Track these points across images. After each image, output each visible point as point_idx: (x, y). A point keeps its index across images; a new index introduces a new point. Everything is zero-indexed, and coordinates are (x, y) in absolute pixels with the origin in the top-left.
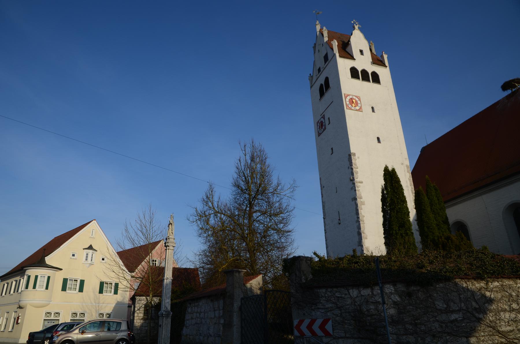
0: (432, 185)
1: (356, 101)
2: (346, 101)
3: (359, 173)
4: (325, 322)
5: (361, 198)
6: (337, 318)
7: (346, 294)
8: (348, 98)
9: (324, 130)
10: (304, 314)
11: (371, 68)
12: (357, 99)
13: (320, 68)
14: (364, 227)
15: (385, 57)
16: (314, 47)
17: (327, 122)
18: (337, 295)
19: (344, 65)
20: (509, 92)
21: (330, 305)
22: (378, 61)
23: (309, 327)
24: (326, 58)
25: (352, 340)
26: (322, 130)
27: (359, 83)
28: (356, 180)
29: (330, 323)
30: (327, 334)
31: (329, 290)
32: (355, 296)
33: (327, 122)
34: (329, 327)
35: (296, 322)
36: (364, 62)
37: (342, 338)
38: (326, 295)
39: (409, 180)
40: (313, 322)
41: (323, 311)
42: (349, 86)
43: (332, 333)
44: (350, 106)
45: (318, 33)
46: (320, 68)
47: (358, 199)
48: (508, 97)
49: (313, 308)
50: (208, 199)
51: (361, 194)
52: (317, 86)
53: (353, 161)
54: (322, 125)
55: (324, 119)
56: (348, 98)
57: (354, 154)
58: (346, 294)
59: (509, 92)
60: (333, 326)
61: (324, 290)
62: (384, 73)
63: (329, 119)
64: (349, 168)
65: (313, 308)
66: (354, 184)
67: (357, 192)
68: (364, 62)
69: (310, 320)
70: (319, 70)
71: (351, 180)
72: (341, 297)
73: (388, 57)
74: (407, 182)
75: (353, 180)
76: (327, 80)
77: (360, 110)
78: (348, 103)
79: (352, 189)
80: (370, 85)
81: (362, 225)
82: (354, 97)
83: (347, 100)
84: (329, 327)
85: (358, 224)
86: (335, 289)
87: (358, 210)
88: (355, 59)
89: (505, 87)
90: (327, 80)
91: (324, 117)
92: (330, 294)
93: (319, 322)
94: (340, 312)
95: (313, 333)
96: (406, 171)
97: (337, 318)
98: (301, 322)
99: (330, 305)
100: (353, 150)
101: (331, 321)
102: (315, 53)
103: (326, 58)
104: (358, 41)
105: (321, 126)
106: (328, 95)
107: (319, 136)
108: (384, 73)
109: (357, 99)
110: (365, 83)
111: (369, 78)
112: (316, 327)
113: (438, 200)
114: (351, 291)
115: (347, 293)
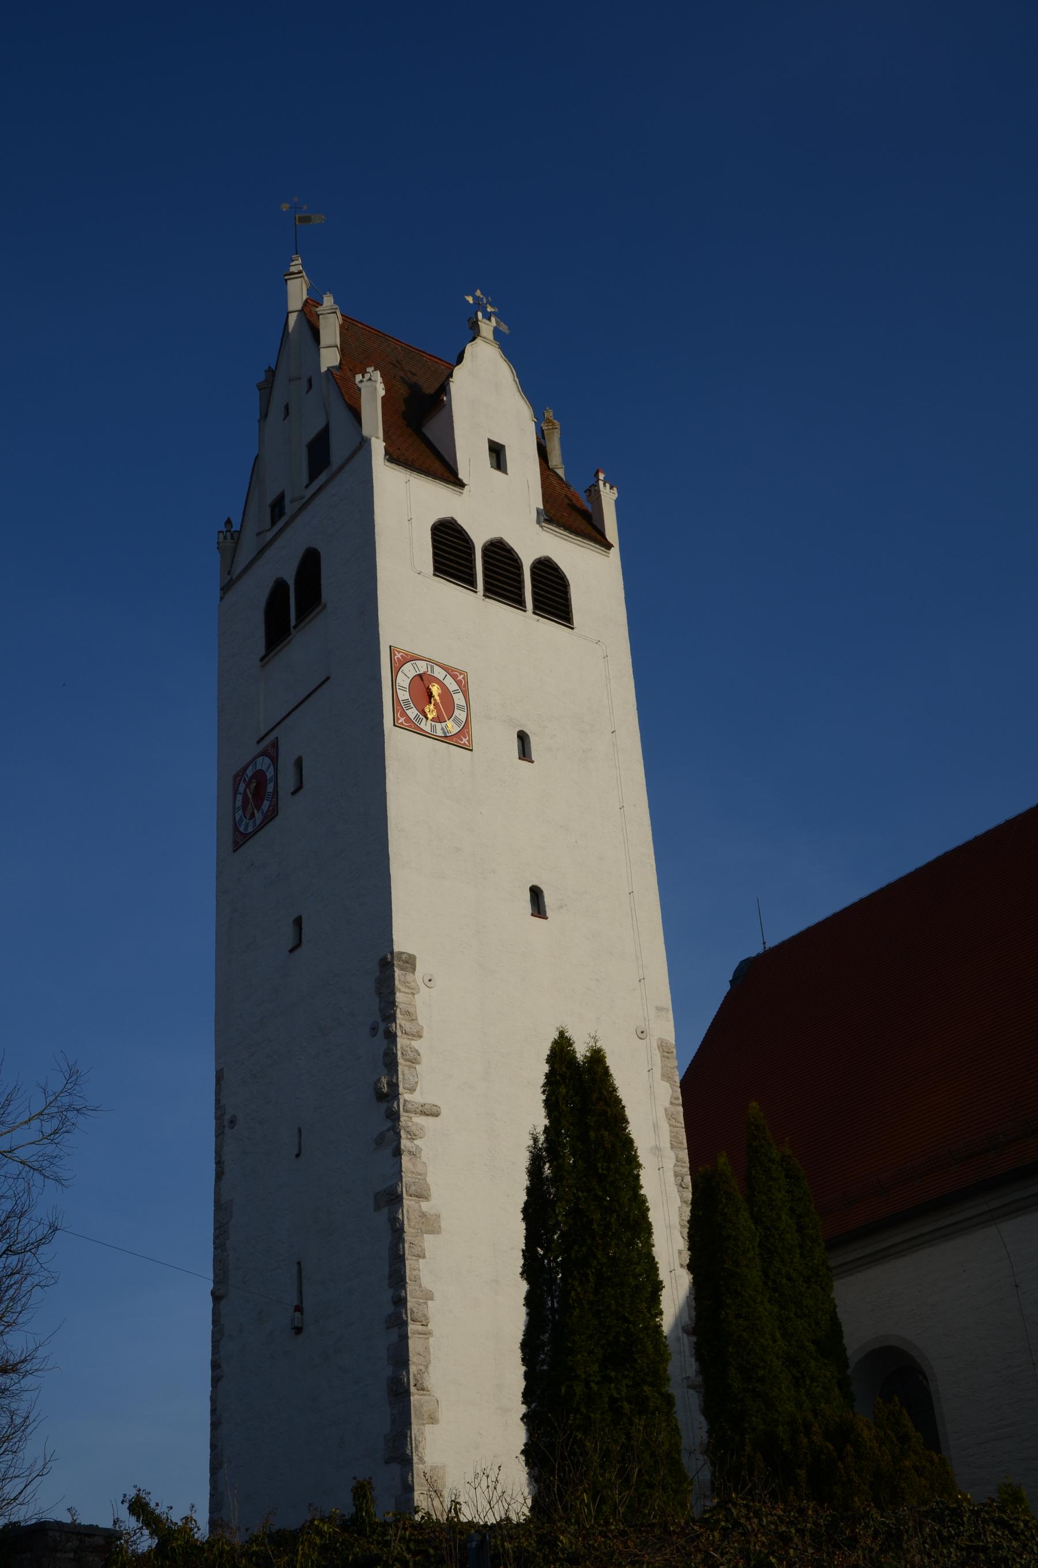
1: (446, 693)
2: (395, 686)
3: (424, 1059)
5: (423, 1195)
8: (409, 671)
11: (534, 544)
12: (451, 685)
15: (608, 497)
17: (287, 781)
24: (319, 453)
26: (259, 816)
27: (468, 606)
28: (405, 1096)
36: (503, 507)
39: (670, 1117)
42: (417, 613)
44: (412, 713)
45: (293, 319)
47: (408, 1202)
51: (423, 1175)
54: (259, 794)
56: (409, 671)
57: (410, 962)
62: (595, 576)
64: (374, 1030)
66: (394, 1117)
67: (405, 1159)
68: (503, 507)
70: (277, 507)
71: (381, 1097)
74: (656, 1127)
75: (393, 1093)
76: (310, 564)
77: (461, 740)
78: (404, 695)
79: (380, 1141)
80: (521, 625)
82: (439, 673)
88: (461, 485)
90: (310, 564)
91: (272, 753)
96: (658, 1071)
102: (264, 415)
103: (319, 453)
105: (253, 797)
106: (305, 644)
107: (237, 846)
110: (500, 611)
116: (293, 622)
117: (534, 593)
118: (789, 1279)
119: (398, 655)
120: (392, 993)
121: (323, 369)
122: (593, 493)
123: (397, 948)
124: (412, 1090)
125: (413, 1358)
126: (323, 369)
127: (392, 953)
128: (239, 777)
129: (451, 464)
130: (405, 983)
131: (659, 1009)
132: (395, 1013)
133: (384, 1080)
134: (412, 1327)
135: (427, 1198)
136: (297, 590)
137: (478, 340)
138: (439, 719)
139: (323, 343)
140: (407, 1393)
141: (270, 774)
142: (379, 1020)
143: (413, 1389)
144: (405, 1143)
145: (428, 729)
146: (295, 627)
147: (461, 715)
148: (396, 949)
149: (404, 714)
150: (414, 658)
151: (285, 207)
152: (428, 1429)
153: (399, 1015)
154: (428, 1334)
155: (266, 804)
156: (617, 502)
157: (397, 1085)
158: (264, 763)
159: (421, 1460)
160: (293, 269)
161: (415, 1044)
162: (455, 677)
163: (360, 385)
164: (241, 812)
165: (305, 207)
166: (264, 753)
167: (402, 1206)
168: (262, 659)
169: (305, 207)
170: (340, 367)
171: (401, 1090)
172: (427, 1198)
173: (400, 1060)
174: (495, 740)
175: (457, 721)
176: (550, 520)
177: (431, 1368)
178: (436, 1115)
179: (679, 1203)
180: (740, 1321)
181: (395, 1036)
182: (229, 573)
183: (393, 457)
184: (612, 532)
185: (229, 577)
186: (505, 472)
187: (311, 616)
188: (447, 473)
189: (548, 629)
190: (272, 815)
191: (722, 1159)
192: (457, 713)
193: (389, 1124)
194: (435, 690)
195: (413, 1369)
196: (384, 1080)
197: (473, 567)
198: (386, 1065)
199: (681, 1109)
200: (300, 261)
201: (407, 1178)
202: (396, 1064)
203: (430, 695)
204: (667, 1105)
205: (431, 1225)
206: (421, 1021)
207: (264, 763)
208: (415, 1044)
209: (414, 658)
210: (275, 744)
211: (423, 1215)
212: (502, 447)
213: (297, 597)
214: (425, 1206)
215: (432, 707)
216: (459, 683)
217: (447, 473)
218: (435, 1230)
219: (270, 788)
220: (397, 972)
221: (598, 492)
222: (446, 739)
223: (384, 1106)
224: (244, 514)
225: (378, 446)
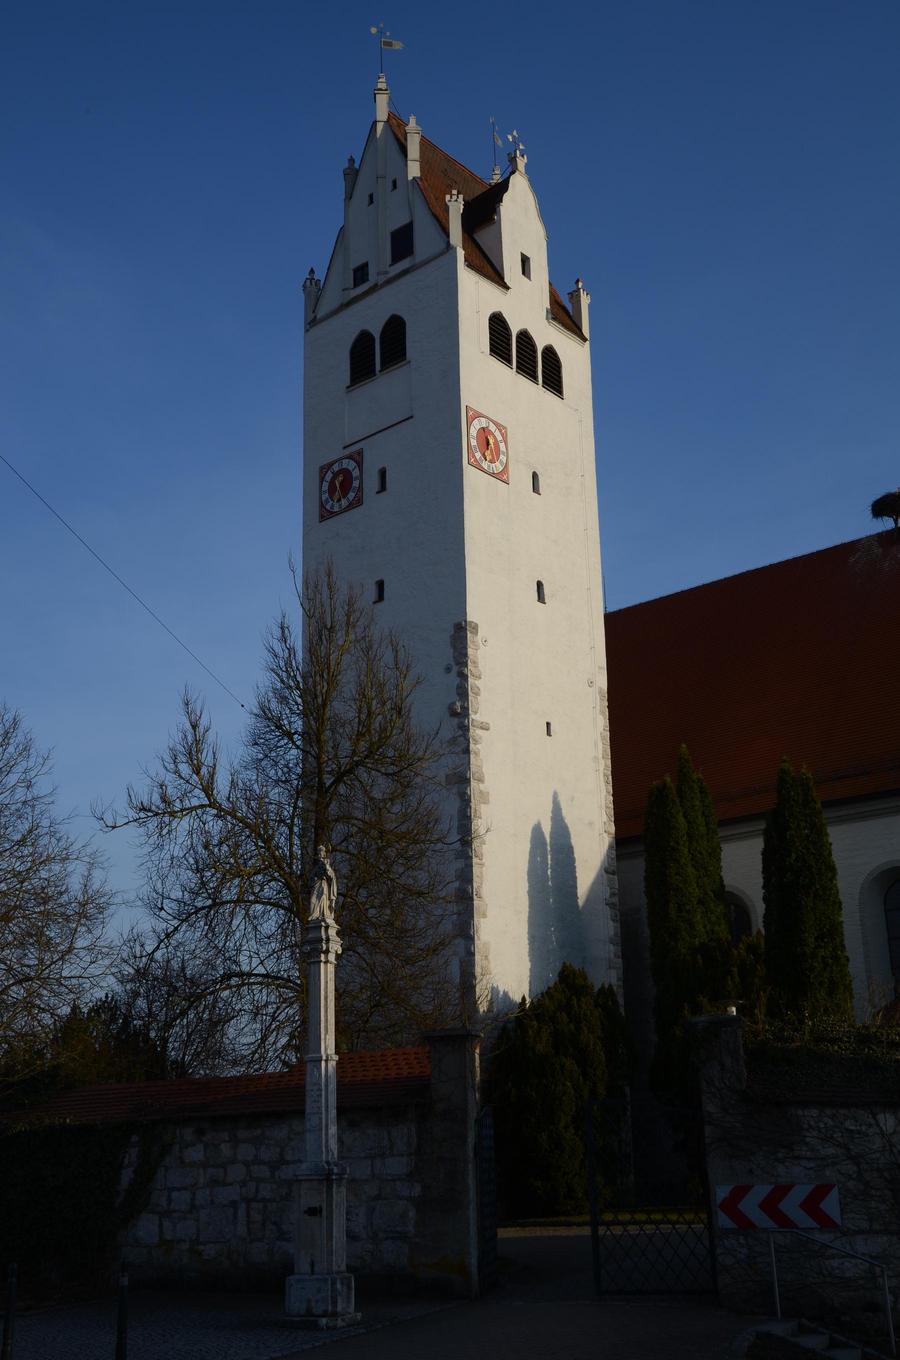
0: (695, 777)
1: (496, 443)
2: (470, 434)
3: (482, 692)
4: (821, 1192)
5: (481, 780)
6: (851, 1184)
7: (870, 1125)
8: (477, 425)
9: (351, 506)
10: (751, 1172)
11: (548, 336)
12: (499, 438)
13: (365, 266)
14: (481, 877)
15: (585, 301)
16: (352, 175)
17: (371, 482)
18: (850, 1125)
19: (475, 297)
20: (887, 524)
21: (831, 1151)
22: (563, 314)
23: (770, 1206)
24: (402, 242)
25: (885, 1238)
26: (344, 502)
27: (506, 376)
28: (472, 716)
29: (834, 1194)
30: (825, 1222)
31: (828, 1111)
32: (891, 1131)
33: (371, 482)
34: (831, 1205)
35: (721, 1193)
36: (527, 306)
37: (862, 1232)
38: (821, 1125)
39: (603, 738)
40: (781, 1191)
41: (811, 1164)
42: (487, 385)
43: (838, 1220)
44: (478, 455)
45: (380, 127)
46: (365, 266)
47: (473, 783)
48: (882, 538)
49: (780, 1155)
50: (193, 751)
51: (480, 767)
52: (344, 330)
53: (470, 651)
54: (346, 486)
55: (360, 464)
56: (477, 425)
57: (475, 628)
58: (870, 1125)
59: (887, 524)
60: (841, 1204)
61: (814, 1112)
62: (575, 358)
63: (383, 474)
64: (448, 669)
65: (780, 1155)
66: (464, 729)
67: (472, 756)
68: (527, 306)
69: (769, 1188)
70: (361, 274)
71: (454, 714)
72: (859, 1132)
73: (590, 306)
74: (596, 744)
75: (465, 713)
76: (395, 329)
77: (501, 476)
78: (474, 442)
79: (453, 741)
80: (533, 392)
81: (476, 870)
82: (492, 428)
83: (474, 432)
84: (831, 1205)
85: (460, 864)
86: (841, 1111)
87: (469, 818)
88: (507, 288)
89: (881, 507)
90: (395, 329)
91: (358, 458)
92: (830, 1123)
93: (800, 1193)
94: (855, 1168)
95: (783, 1221)
96: (598, 708)
97: (851, 1184)
98: (740, 1192)
99: (831, 1151)
100: (473, 614)
101: (835, 1191)
102: (349, 197)
103: (402, 242)
104: (521, 222)
105: (337, 488)
106: (386, 386)
107: (322, 518)
108: (575, 358)
109: (499, 438)
110: (524, 382)
111: (535, 367)
112: (791, 1206)
113: (707, 824)
114: (881, 1117)
115: (872, 1121)
116: (378, 367)
117: (543, 371)
118: (700, 853)
119: (471, 413)
120: (465, 647)
121: (410, 178)
122: (574, 296)
123: (469, 619)
124: (476, 713)
125: (475, 878)
126: (410, 178)
127: (466, 621)
128: (324, 470)
129: (499, 269)
130: (473, 642)
131: (600, 668)
132: (467, 662)
133: (458, 704)
134: (475, 860)
135: (483, 782)
136: (382, 343)
137: (517, 173)
138: (492, 461)
139: (409, 157)
140: (472, 899)
141: (356, 473)
142: (453, 664)
143: (475, 897)
144: (472, 747)
145: (486, 467)
146: (380, 371)
147: (503, 458)
148: (468, 619)
149: (474, 456)
150: (480, 415)
151: (374, 30)
152: (482, 920)
153: (469, 663)
154: (483, 865)
155: (351, 495)
156: (589, 305)
157: (468, 709)
158: (351, 465)
159: (479, 938)
160: (380, 86)
161: (477, 682)
162: (500, 431)
163: (448, 204)
164: (327, 495)
165: (388, 33)
166: (350, 457)
167: (470, 785)
168: (348, 388)
169: (388, 33)
170: (421, 178)
171: (470, 712)
172: (483, 782)
173: (470, 693)
174: (521, 478)
175: (501, 462)
176: (554, 319)
177: (483, 885)
178: (488, 729)
179: (605, 793)
180: (678, 877)
181: (467, 677)
182: (314, 312)
183: (470, 264)
184: (586, 331)
185: (313, 315)
186: (529, 277)
187: (395, 367)
188: (496, 276)
189: (549, 397)
190: (358, 502)
191: (668, 779)
192: (501, 456)
193: (460, 732)
194: (491, 441)
195: (475, 885)
196: (458, 704)
197: (510, 350)
198: (459, 694)
199: (608, 733)
200: (384, 80)
201: (473, 768)
202: (467, 695)
203: (488, 443)
204: (602, 730)
205: (485, 798)
206: (481, 668)
207: (351, 465)
208: (477, 682)
209: (480, 415)
210: (360, 453)
211: (481, 792)
212: (528, 259)
213: (382, 348)
214: (482, 786)
215: (489, 452)
216: (502, 435)
217: (496, 276)
218: (486, 802)
219: (356, 484)
220: (469, 635)
221: (579, 297)
222: (493, 475)
223: (455, 721)
224: (328, 269)
225: (461, 254)
